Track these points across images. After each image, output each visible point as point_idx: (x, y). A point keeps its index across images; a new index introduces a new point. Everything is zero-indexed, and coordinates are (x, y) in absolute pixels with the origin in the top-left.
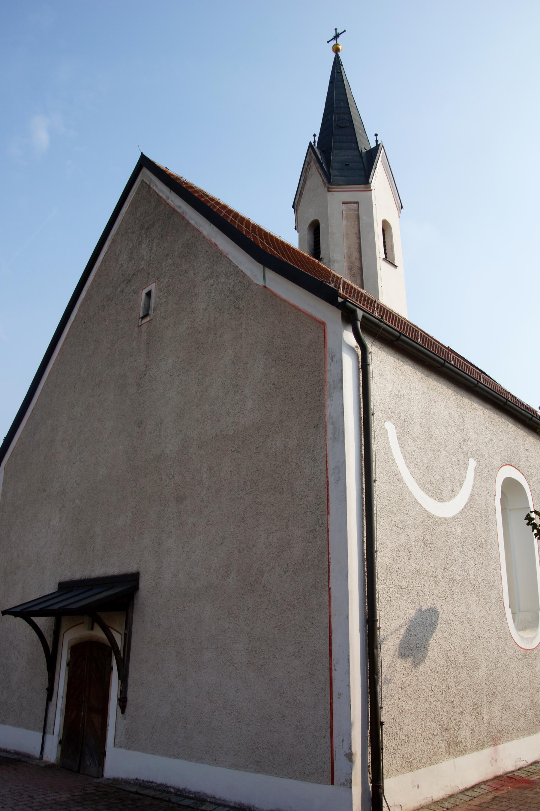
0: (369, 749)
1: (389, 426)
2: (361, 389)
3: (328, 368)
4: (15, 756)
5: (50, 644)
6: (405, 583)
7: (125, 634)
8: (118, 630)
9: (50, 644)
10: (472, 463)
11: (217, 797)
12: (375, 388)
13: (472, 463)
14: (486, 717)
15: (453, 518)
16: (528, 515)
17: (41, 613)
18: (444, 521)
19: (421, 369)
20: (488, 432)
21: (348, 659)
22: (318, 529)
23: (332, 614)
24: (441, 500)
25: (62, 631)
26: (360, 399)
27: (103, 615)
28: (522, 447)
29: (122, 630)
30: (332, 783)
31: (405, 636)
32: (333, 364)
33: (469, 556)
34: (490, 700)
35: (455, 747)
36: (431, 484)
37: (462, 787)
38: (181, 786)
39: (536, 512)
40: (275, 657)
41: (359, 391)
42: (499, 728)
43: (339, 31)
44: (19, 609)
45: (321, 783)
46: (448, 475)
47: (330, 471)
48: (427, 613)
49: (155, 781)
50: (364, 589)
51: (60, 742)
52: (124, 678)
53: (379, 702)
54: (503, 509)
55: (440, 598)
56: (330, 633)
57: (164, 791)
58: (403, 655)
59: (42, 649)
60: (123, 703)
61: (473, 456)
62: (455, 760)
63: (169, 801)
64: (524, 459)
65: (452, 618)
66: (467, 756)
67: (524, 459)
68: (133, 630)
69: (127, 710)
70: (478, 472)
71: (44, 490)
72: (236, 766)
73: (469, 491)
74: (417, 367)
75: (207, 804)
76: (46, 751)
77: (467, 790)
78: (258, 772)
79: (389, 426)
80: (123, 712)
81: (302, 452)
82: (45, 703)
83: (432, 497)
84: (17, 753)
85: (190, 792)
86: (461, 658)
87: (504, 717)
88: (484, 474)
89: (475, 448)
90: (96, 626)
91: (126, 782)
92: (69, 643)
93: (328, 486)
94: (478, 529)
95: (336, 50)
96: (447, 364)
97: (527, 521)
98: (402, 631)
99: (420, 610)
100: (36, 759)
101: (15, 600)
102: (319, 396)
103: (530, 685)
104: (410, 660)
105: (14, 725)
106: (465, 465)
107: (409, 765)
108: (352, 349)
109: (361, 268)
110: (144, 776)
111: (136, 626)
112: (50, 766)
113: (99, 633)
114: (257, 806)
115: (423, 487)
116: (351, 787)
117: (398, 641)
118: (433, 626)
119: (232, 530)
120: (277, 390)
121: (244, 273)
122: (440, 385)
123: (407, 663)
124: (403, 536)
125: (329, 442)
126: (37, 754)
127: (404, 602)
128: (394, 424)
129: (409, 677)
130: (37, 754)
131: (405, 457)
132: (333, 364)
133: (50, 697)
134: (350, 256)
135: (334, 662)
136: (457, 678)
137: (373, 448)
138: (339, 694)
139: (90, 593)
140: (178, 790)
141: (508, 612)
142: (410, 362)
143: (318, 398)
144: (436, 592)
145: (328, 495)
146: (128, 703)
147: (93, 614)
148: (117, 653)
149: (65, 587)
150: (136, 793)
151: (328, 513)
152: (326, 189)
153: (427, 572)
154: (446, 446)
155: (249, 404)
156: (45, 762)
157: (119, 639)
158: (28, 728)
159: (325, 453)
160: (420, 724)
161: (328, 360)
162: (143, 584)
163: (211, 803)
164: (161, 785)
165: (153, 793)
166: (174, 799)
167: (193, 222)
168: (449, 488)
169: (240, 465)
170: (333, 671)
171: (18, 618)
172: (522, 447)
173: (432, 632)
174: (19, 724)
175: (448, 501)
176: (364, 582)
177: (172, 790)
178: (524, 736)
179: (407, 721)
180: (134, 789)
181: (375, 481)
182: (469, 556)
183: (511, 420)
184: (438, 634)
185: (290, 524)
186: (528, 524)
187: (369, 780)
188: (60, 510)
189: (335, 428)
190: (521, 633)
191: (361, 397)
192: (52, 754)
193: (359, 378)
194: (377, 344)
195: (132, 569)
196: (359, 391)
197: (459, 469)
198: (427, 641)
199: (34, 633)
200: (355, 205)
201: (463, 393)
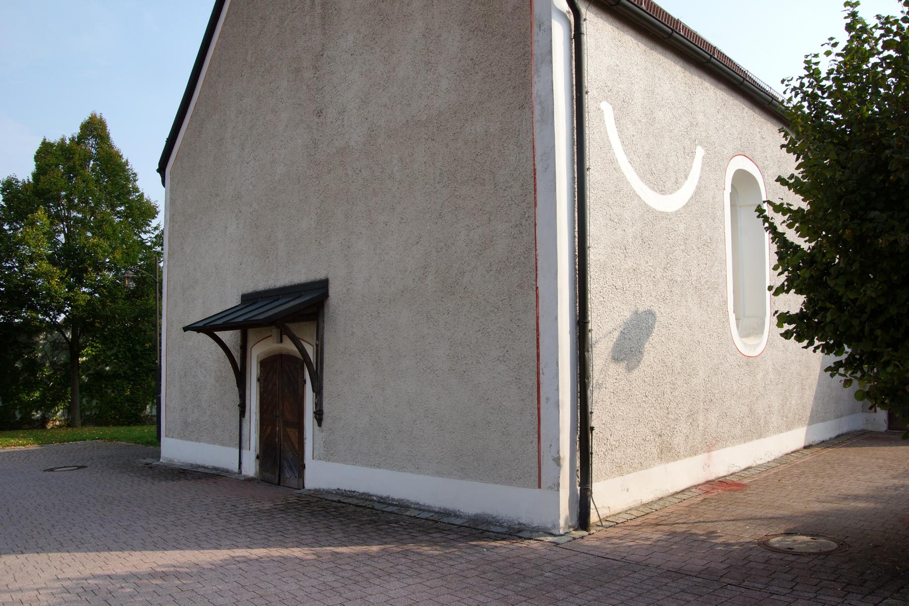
0: (578, 454)
1: (606, 107)
2: (574, 63)
3: (535, 38)
4: (214, 472)
5: (238, 360)
6: (620, 283)
7: (317, 345)
9: (238, 360)
10: (700, 152)
11: (422, 503)
12: (590, 61)
13: (700, 152)
14: (701, 424)
15: (676, 213)
16: (759, 206)
17: (225, 327)
18: (665, 216)
19: (644, 40)
20: (720, 116)
21: (557, 362)
22: (524, 222)
23: (540, 315)
24: (663, 192)
25: (249, 345)
26: (572, 74)
27: (293, 327)
28: (758, 135)
29: (314, 342)
30: (540, 487)
31: (619, 340)
32: (540, 33)
33: (693, 255)
34: (707, 407)
35: (667, 453)
36: (652, 174)
37: (672, 491)
38: (384, 494)
39: (769, 202)
40: (478, 362)
41: (571, 65)
42: (715, 435)
44: (201, 324)
45: (528, 487)
46: (671, 164)
47: (537, 159)
48: (643, 316)
50: (575, 288)
51: (258, 457)
52: (318, 390)
53: (590, 407)
54: (733, 205)
55: (658, 300)
56: (538, 335)
57: (367, 500)
58: (616, 359)
59: (230, 365)
60: (319, 415)
61: (701, 144)
62: (668, 465)
63: (373, 508)
64: (759, 149)
65: (671, 321)
66: (679, 462)
67: (759, 149)
68: (325, 340)
69: (324, 423)
70: (706, 163)
71: (217, 195)
72: (439, 474)
73: (696, 183)
74: (639, 37)
75: (412, 510)
76: (243, 465)
77: (677, 493)
78: (463, 478)
79: (606, 107)
80: (320, 425)
81: (505, 137)
82: (238, 419)
83: (653, 188)
84: (216, 469)
85: (393, 500)
86: (678, 364)
87: (721, 424)
88: (713, 164)
89: (704, 134)
90: (285, 338)
91: (328, 492)
92: (258, 357)
93: (535, 174)
94: (704, 225)
96: (675, 35)
97: (758, 213)
98: (616, 334)
99: (636, 313)
100: (235, 473)
101: (196, 317)
102: (525, 71)
103: (750, 393)
104: (624, 364)
105: (209, 442)
106: (693, 153)
107: (620, 469)
108: (563, 15)
110: (346, 486)
111: (328, 336)
112: (250, 480)
113: (289, 346)
114: (462, 510)
115: (642, 177)
116: (558, 490)
117: (611, 344)
118: (649, 330)
119: (429, 228)
120: (476, 67)
122: (666, 60)
123: (621, 368)
124: (619, 231)
125: (537, 126)
126: (235, 468)
127: (618, 304)
128: (611, 104)
129: (622, 382)
130: (235, 468)
131: (623, 142)
132: (540, 33)
133: (242, 413)
135: (541, 366)
136: (674, 384)
137: (586, 115)
138: (547, 399)
139: (276, 303)
140: (381, 498)
141: (732, 317)
142: (632, 32)
143: (523, 75)
144: (654, 294)
145: (535, 185)
146: (325, 416)
147: (281, 324)
148: (309, 364)
149: (249, 299)
150: (339, 502)
151: (536, 206)
153: (645, 271)
154: (671, 131)
155: (444, 84)
156: (245, 476)
157: (310, 351)
158: (223, 445)
159: (531, 137)
160: (632, 430)
161: (535, 29)
162: (334, 291)
163: (416, 509)
164: (363, 494)
165: (355, 501)
166: (377, 506)
168: (673, 179)
169: (435, 154)
170: (541, 375)
171: (201, 334)
172: (758, 135)
173: (648, 336)
174: (214, 441)
175: (671, 193)
176: (575, 281)
178: (739, 443)
179: (618, 427)
180: (336, 499)
181: (588, 169)
182: (693, 255)
183: (747, 103)
184: (654, 338)
185: (492, 218)
186: (758, 217)
187: (578, 484)
188: (237, 216)
189: (543, 108)
190: (744, 340)
191: (574, 72)
192: (251, 468)
193: (571, 50)
194: (593, 9)
195: (316, 275)
196: (571, 65)
197: (685, 158)
198: (643, 345)
199: (220, 350)
201: (693, 69)
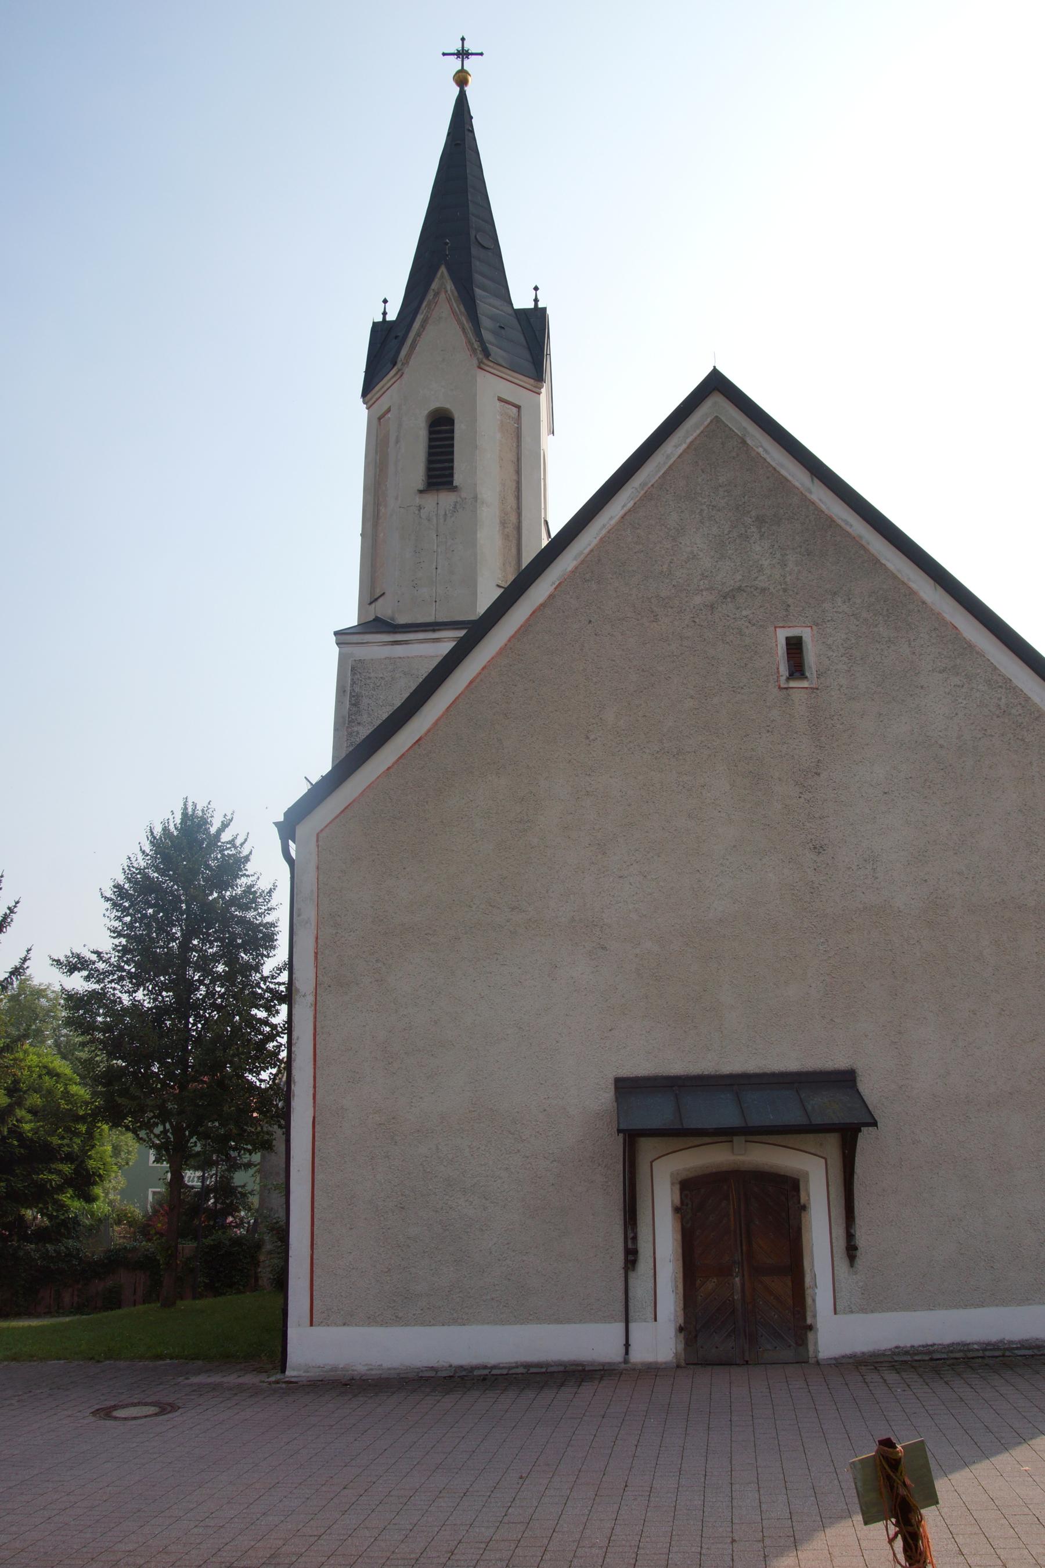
8: (813, 1151)
43: (469, 46)
49: (936, 1342)
69: (859, 1262)
95: (461, 79)
109: (519, 528)
112: (652, 1371)
121: (1004, 676)
134: (503, 500)
152: (475, 362)
167: (889, 565)
177: (976, 1346)
200: (515, 410)
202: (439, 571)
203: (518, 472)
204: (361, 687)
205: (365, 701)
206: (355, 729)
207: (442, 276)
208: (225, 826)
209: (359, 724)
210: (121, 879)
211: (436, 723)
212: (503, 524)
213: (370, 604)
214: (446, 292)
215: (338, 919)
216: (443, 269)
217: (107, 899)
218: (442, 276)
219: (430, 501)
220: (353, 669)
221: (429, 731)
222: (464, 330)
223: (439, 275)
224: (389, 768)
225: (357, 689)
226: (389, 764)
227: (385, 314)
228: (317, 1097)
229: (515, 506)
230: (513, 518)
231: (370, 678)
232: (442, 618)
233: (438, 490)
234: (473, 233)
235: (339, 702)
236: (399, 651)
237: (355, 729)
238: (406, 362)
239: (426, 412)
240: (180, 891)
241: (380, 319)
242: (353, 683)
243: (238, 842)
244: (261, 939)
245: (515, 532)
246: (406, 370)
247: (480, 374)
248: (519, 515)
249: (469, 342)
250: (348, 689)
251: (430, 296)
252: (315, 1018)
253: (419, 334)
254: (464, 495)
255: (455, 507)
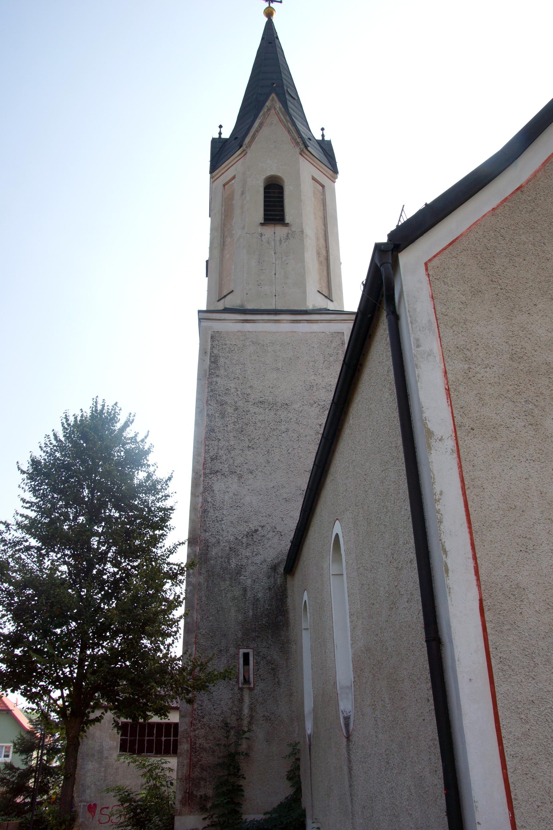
152: (298, 150)
202: (277, 276)
203: (325, 225)
204: (218, 351)
205: (222, 361)
206: (215, 379)
207: (273, 100)
208: (126, 425)
209: (217, 376)
210: (40, 455)
211: (535, 175)
212: (318, 254)
213: (219, 301)
214: (275, 109)
215: (469, 354)
216: (273, 95)
217: (23, 472)
218: (273, 100)
219: (269, 231)
220: (212, 337)
221: (528, 181)
222: (289, 132)
223: (271, 98)
224: (494, 209)
225: (216, 352)
226: (494, 204)
227: (220, 134)
228: (481, 571)
229: (324, 245)
230: (324, 252)
231: (225, 344)
232: (280, 306)
233: (275, 224)
234: (285, 88)
235: (201, 360)
236: (248, 327)
237: (215, 379)
238: (249, 145)
239: (264, 177)
240: (85, 474)
241: (217, 136)
242: (213, 347)
243: (139, 439)
244: (162, 521)
245: (325, 262)
246: (249, 151)
247: (301, 159)
248: (327, 251)
249: (293, 139)
250: (209, 351)
251: (265, 109)
252: (460, 467)
253: (257, 131)
254: (293, 229)
255: (287, 236)
